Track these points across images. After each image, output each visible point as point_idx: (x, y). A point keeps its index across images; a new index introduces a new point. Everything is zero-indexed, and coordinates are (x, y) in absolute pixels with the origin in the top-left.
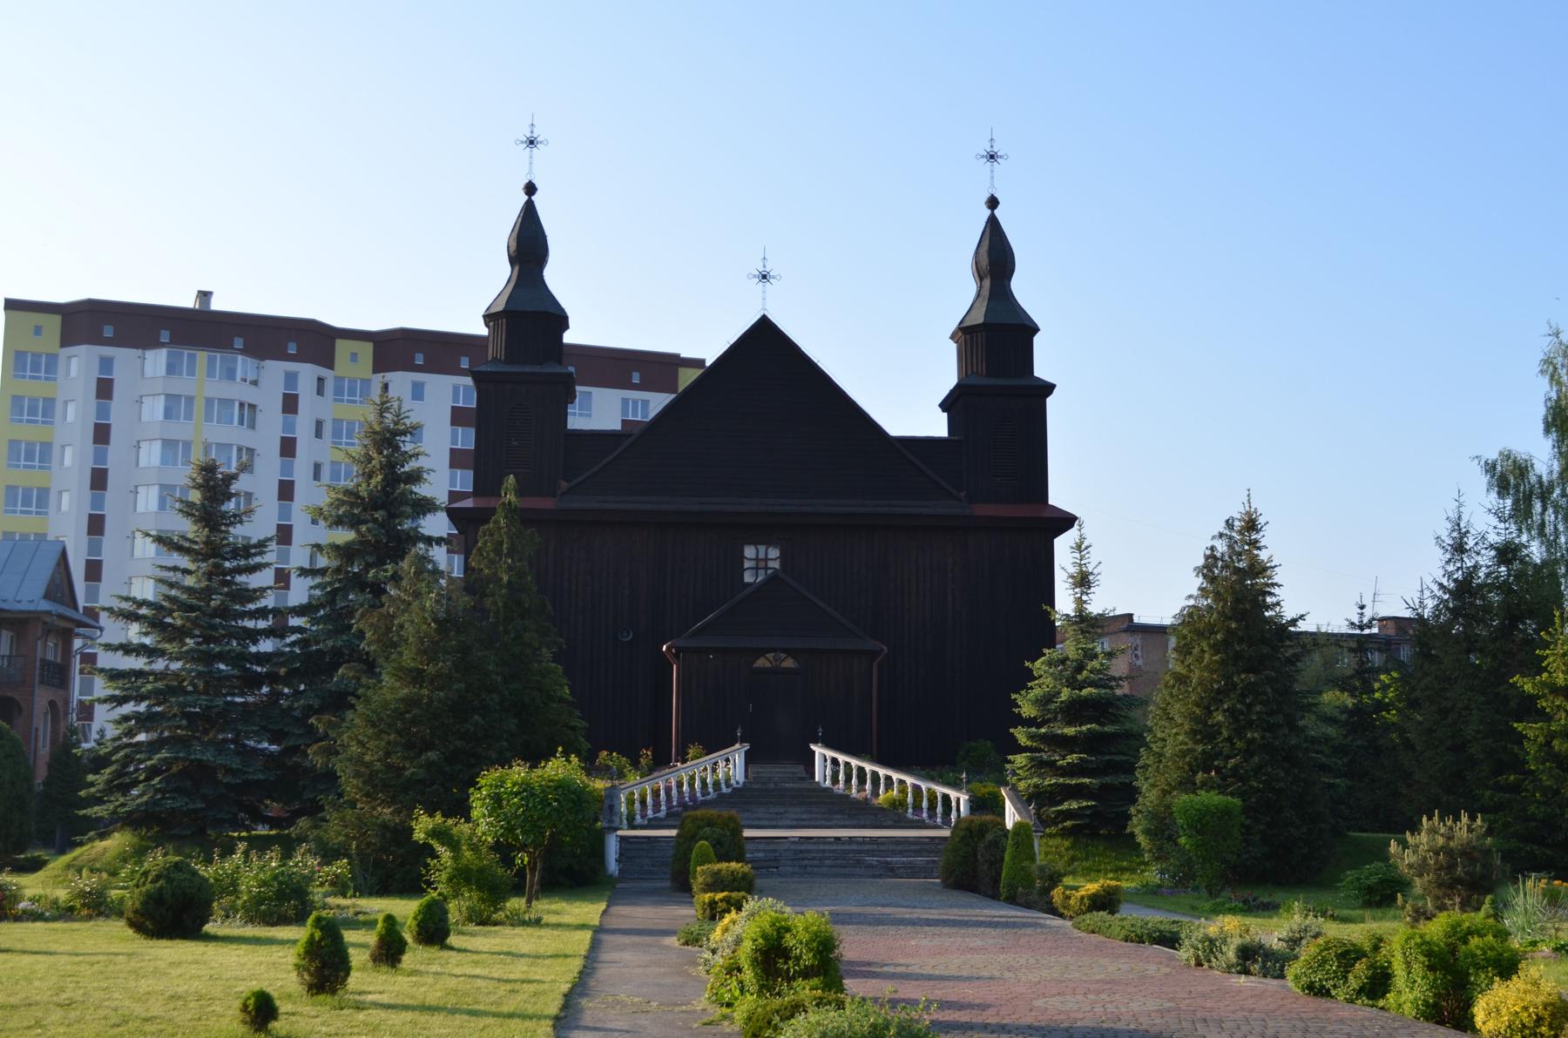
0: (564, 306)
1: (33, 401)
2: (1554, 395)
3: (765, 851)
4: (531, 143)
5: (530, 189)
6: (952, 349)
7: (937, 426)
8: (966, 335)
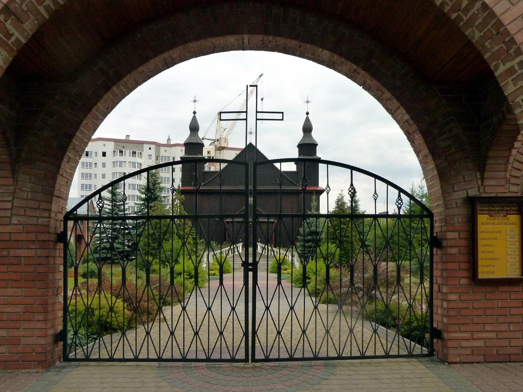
0: (387, 113)
4: (195, 101)
5: (195, 113)
6: (297, 149)
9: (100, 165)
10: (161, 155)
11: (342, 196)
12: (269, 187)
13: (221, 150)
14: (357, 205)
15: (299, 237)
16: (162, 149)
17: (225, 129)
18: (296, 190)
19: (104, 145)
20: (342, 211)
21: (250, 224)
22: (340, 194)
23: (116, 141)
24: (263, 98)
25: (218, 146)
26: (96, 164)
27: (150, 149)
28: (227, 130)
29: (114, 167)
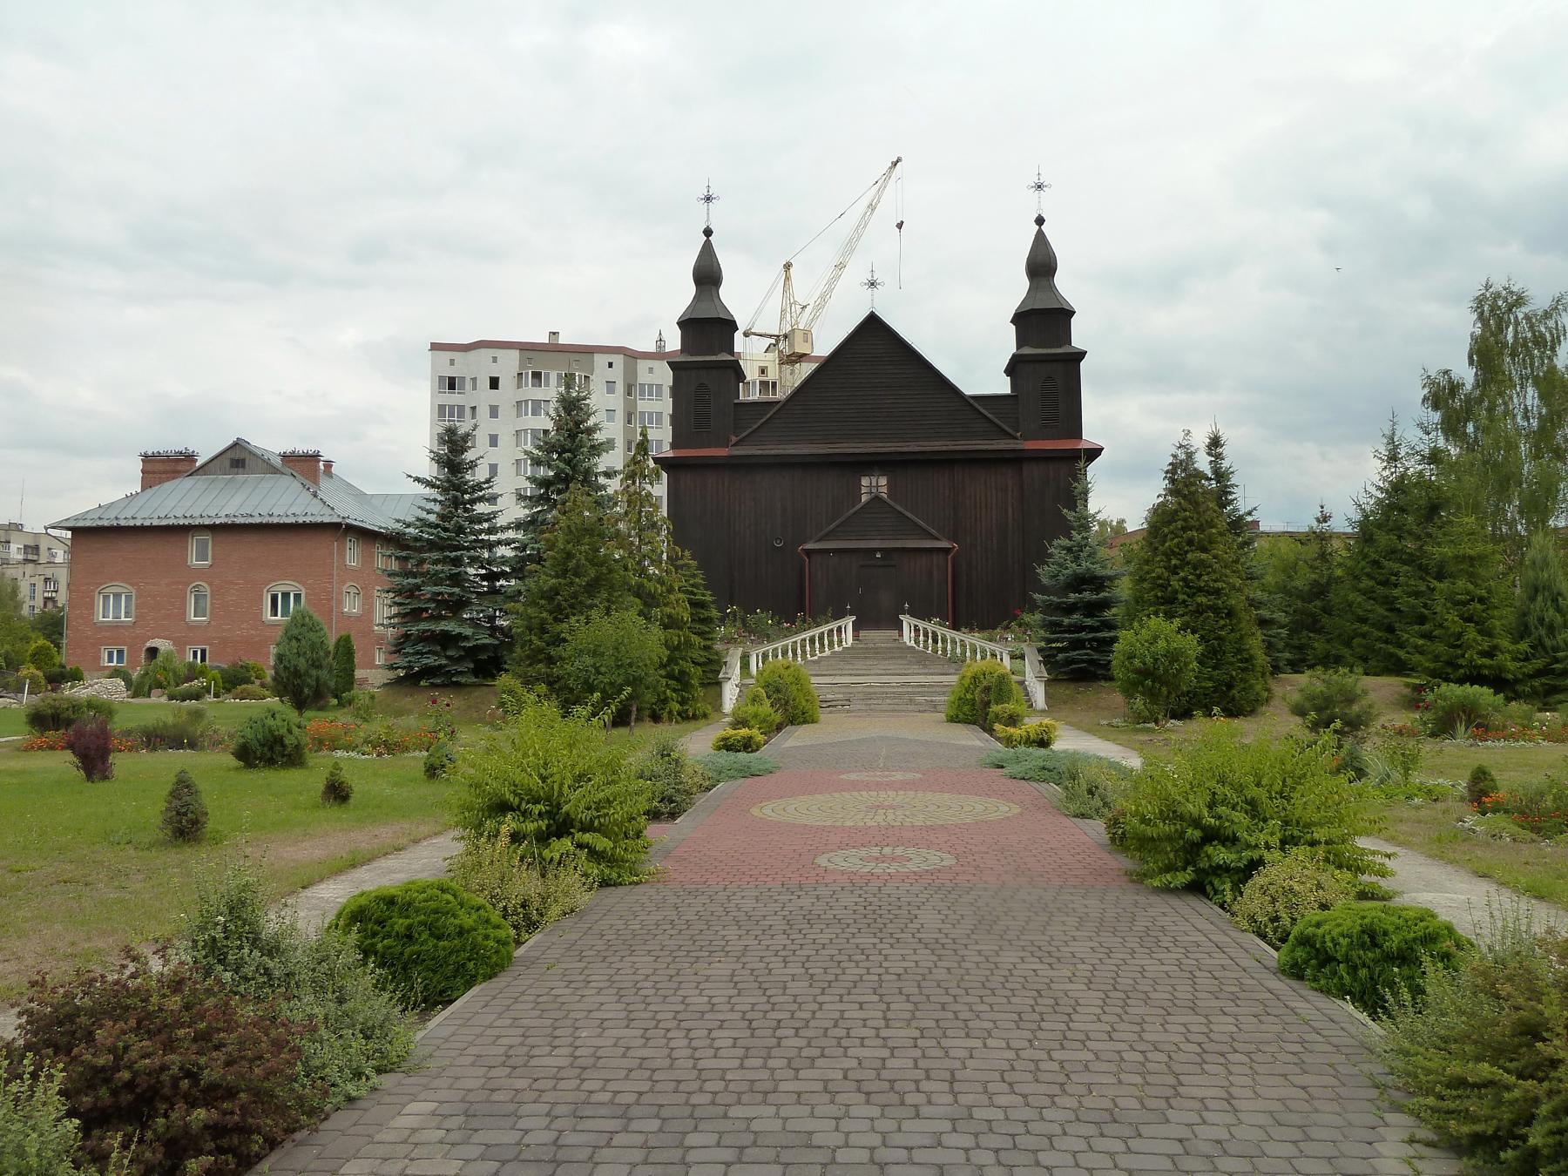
1: (452, 407)
2: (1478, 331)
3: (843, 693)
4: (872, 284)
5: (708, 232)
7: (1003, 386)
8: (1022, 319)
9: (483, 412)
10: (640, 380)
11: (1187, 453)
12: (932, 443)
13: (793, 363)
14: (1227, 486)
15: (1036, 596)
16: (642, 365)
17: (805, 307)
18: (1014, 450)
19: (495, 360)
20: (1190, 503)
21: (878, 556)
22: (1181, 446)
23: (526, 348)
24: (902, 222)
25: (787, 352)
26: (474, 408)
27: (610, 365)
28: (808, 309)
29: (519, 415)
